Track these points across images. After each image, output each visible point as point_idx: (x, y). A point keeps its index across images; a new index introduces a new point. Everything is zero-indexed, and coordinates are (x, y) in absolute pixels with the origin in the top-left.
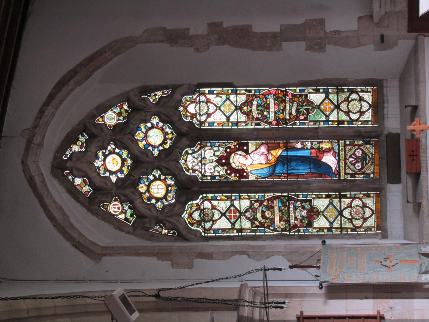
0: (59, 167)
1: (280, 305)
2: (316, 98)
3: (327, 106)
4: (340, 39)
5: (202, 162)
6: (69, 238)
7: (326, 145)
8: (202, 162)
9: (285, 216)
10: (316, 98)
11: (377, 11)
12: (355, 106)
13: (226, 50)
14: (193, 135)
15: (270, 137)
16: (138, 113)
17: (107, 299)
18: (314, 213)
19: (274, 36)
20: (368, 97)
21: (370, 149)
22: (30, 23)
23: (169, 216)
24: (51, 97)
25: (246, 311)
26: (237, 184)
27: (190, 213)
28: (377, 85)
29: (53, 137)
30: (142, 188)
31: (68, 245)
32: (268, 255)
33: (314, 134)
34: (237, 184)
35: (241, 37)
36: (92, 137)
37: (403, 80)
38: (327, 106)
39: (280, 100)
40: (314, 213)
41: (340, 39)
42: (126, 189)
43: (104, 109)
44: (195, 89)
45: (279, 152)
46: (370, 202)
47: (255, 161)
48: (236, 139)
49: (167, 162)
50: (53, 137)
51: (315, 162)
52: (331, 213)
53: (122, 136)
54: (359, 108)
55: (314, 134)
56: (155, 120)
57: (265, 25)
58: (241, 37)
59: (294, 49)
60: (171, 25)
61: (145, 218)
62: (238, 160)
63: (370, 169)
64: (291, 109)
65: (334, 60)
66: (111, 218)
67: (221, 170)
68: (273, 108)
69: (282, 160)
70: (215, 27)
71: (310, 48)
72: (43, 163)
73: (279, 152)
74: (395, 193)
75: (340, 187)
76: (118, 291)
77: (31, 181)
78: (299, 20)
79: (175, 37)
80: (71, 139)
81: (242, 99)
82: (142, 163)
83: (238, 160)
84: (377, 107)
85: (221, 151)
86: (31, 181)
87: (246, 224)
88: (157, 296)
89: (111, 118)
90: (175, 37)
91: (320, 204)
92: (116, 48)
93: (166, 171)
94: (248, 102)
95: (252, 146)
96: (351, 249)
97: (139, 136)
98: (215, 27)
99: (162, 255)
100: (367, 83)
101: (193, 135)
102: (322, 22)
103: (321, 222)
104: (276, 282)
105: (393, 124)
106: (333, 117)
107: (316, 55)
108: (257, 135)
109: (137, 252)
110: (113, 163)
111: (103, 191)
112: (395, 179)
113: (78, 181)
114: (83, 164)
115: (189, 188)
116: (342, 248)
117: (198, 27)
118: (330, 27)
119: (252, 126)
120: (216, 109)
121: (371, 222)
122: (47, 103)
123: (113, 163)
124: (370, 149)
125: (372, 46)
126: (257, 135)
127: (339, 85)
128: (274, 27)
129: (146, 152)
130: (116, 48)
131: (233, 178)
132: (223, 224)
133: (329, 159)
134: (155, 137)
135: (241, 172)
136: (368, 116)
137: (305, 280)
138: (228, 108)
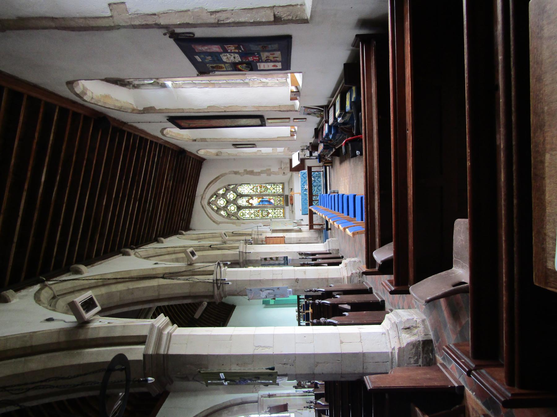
0: (209, 203)
1: (261, 235)
2: (269, 187)
3: (272, 189)
4: (275, 173)
5: (242, 202)
6: (212, 220)
7: (271, 198)
8: (242, 202)
9: (262, 214)
10: (269, 187)
11: (283, 167)
12: (278, 189)
13: (248, 176)
14: (241, 196)
15: (258, 196)
16: (227, 190)
17: (221, 234)
18: (268, 213)
19: (259, 172)
20: (281, 187)
21: (281, 198)
22: (202, 170)
23: (235, 214)
24: (207, 187)
25: (253, 236)
26: (251, 207)
27: (240, 213)
28: (283, 184)
29: (208, 196)
30: (229, 208)
31: (211, 221)
32: (258, 223)
33: (268, 195)
34: (251, 207)
35: (251, 173)
36: (217, 196)
37: (289, 182)
38: (272, 189)
39: (261, 187)
40: (268, 213)
41: (275, 173)
42: (225, 208)
43: (219, 190)
44: (241, 185)
45: (260, 199)
46: (282, 211)
47: (255, 202)
48: (251, 197)
49: (235, 202)
50: (208, 196)
51: (269, 202)
52: (273, 213)
53: (224, 196)
54: (279, 189)
55: (268, 195)
56: (232, 192)
57: (256, 170)
58: (251, 173)
59: (264, 176)
60: (235, 170)
61: (229, 215)
62: (251, 201)
63: (281, 203)
64: (263, 189)
65: (273, 178)
66: (221, 215)
67: (247, 204)
68: (259, 189)
69: (262, 201)
70: (245, 170)
71: (268, 175)
72: (205, 202)
73: (260, 199)
74: (287, 209)
75: (275, 208)
76: (223, 232)
77: (203, 207)
78: (265, 169)
79: (236, 173)
80: (212, 197)
81: (252, 187)
82: (228, 202)
83: (251, 201)
84: (283, 189)
85: (247, 199)
86: (203, 207)
87: (253, 216)
88: (210, 246)
89: (221, 192)
90: (236, 173)
91: (270, 211)
92: (222, 176)
93: (235, 204)
94: (253, 188)
95: (254, 198)
96: (277, 222)
97: (228, 196)
98: (245, 170)
99: (233, 223)
100: (281, 183)
101: (241, 196)
102: (270, 169)
103: (270, 215)
104: (260, 229)
105: (287, 193)
106: (273, 191)
107: (268, 177)
108: (255, 195)
109: (228, 223)
110: (222, 202)
111: (219, 209)
112: (287, 205)
113: (214, 207)
114: (215, 203)
115: (239, 208)
116: (275, 221)
117: (241, 171)
118: (272, 171)
119: (254, 193)
120: (245, 189)
121: (282, 215)
122: (206, 188)
123: (222, 202)
124: (281, 198)
125: (292, 312)
126: (255, 195)
127: (274, 184)
128: (258, 170)
129: (229, 200)
130: (222, 176)
131: (250, 205)
132: (248, 216)
133: (272, 201)
134: (231, 196)
135: (252, 204)
136: (281, 191)
137: (267, 229)
138: (249, 189)
